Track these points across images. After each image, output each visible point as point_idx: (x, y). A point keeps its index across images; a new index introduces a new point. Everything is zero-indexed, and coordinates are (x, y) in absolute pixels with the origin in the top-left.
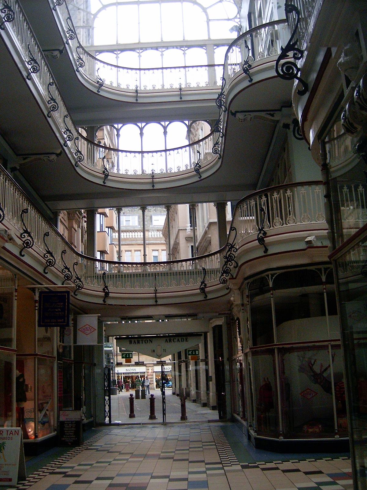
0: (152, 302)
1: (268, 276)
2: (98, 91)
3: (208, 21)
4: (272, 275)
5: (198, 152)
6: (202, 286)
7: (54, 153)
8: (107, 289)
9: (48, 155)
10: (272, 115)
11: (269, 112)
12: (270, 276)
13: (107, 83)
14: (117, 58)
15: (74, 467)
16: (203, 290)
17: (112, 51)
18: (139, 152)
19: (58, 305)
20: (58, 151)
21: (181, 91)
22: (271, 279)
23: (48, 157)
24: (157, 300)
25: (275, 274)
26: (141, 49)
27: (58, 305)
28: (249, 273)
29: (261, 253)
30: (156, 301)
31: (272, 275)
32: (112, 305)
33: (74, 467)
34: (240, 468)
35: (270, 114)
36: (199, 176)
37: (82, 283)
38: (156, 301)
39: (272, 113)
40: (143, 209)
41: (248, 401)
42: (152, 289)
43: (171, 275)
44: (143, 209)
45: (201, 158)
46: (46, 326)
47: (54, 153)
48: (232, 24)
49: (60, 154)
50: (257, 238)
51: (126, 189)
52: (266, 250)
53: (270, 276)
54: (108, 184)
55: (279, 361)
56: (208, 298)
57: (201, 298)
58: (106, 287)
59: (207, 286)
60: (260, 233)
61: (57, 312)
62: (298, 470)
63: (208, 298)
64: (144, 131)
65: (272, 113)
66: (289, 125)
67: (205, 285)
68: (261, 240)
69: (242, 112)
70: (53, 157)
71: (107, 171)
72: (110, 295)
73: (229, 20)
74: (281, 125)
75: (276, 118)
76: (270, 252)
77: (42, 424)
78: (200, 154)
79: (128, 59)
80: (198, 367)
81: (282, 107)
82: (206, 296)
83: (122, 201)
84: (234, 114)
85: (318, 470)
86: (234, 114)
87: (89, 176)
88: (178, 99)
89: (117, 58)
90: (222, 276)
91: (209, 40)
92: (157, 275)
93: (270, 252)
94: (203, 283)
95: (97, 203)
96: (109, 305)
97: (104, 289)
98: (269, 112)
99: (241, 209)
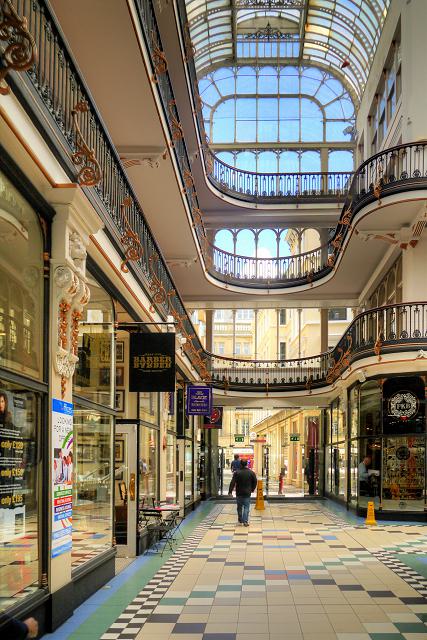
3: (325, 121)
14: (235, 158)
15: (122, 629)
17: (230, 151)
18: (254, 259)
26: (258, 149)
33: (122, 629)
34: (327, 567)
40: (256, 311)
44: (256, 311)
46: (106, 335)
48: (346, 125)
55: (42, 229)
62: (351, 549)
73: (344, 120)
77: (212, 421)
79: (246, 161)
80: (396, 600)
83: (238, 304)
85: (385, 589)
89: (235, 158)
91: (325, 142)
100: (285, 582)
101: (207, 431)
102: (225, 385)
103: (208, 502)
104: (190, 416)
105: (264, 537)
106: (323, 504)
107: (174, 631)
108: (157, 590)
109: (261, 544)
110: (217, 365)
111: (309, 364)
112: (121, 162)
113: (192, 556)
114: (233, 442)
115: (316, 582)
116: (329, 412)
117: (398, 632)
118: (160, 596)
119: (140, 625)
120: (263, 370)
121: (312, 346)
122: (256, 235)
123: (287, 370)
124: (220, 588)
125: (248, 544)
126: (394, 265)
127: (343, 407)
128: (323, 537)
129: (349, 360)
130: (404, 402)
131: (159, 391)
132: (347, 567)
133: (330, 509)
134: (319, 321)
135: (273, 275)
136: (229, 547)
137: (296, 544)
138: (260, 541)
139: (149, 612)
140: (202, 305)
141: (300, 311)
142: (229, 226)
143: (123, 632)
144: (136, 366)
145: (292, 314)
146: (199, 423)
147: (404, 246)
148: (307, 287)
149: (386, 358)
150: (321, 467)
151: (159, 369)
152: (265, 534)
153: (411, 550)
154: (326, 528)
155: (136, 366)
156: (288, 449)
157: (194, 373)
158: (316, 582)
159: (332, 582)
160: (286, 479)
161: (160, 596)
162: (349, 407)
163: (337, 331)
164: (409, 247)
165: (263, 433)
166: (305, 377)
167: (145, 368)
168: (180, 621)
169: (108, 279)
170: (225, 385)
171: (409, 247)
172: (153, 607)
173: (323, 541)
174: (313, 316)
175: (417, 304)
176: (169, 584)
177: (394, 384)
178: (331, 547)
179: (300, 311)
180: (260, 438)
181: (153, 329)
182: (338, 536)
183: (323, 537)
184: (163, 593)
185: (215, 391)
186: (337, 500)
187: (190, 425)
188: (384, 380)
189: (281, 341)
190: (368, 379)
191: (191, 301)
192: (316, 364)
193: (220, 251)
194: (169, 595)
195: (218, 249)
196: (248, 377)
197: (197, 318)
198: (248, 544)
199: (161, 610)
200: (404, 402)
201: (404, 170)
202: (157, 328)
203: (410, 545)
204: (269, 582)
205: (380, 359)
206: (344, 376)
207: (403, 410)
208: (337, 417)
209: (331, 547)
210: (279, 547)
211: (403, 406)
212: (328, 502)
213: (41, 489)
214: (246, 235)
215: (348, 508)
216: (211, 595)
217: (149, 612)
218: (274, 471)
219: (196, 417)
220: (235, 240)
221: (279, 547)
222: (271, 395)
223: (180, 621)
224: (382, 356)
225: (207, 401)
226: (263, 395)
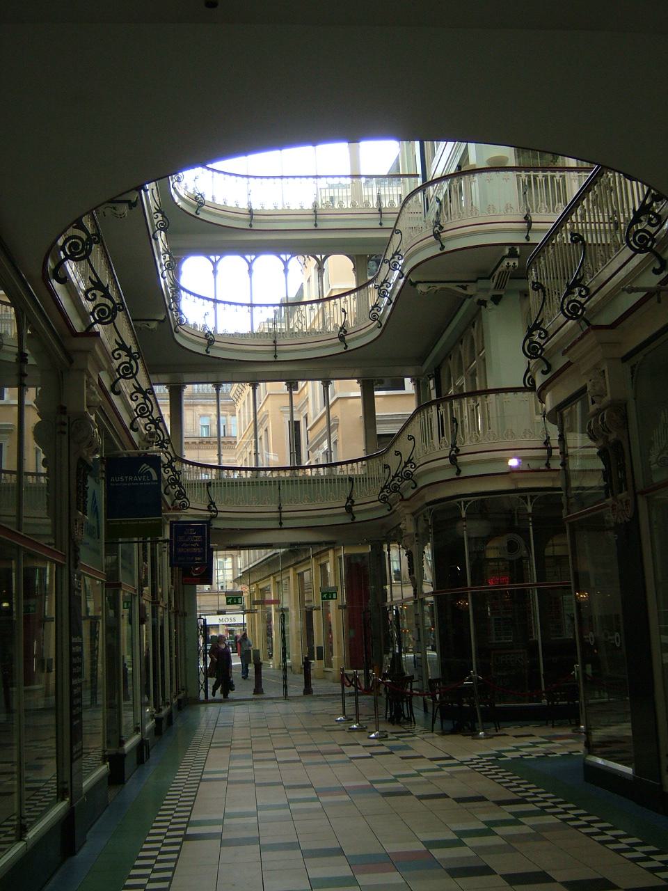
0: (275, 524)
1: (460, 503)
2: (196, 212)
4: (466, 503)
5: (344, 311)
6: (341, 333)
7: (154, 320)
8: (215, 507)
9: (148, 322)
10: (465, 288)
11: (460, 284)
12: (463, 503)
13: (208, 198)
16: (349, 509)
19: (195, 539)
20: (162, 317)
21: (316, 214)
22: (465, 507)
23: (148, 325)
24: (282, 521)
25: (470, 501)
27: (195, 539)
28: (429, 498)
29: (451, 474)
30: (281, 524)
31: (466, 503)
32: (219, 529)
33: (165, 838)
35: (462, 287)
36: (344, 346)
37: (188, 501)
38: (281, 524)
39: (465, 284)
41: (126, 647)
42: (275, 507)
43: (292, 484)
45: (346, 319)
47: (154, 320)
49: (163, 321)
50: (448, 455)
51: (237, 360)
52: (459, 471)
53: (463, 503)
54: (213, 353)
56: (356, 520)
57: (347, 519)
58: (213, 503)
59: (355, 504)
60: (452, 450)
61: (193, 547)
62: (432, 759)
63: (356, 520)
64: (254, 267)
65: (465, 284)
66: (486, 301)
67: (353, 501)
68: (453, 459)
69: (425, 282)
70: (154, 325)
71: (211, 334)
72: (220, 515)
74: (476, 300)
75: (469, 292)
76: (462, 475)
78: (345, 314)
81: (479, 278)
82: (354, 517)
84: (414, 284)
86: (414, 284)
87: (196, 346)
88: (312, 226)
90: (381, 493)
92: (281, 483)
93: (462, 475)
94: (350, 498)
95: (186, 377)
96: (215, 528)
97: (209, 507)
98: (460, 284)
99: (424, 415)
100: (346, 798)
115: (386, 794)
117: (457, 838)
122: (250, 264)
132: (426, 777)
138: (298, 758)
140: (165, 378)
142: (206, 251)
147: (482, 303)
153: (516, 755)
158: (386, 794)
159: (408, 793)
164: (490, 305)
169: (23, 427)
171: (490, 305)
178: (402, 758)
183: (389, 747)
191: (190, 372)
193: (191, 293)
201: (336, 322)
203: (517, 749)
204: (322, 799)
208: (396, 559)
209: (402, 758)
213: (245, 349)
214: (232, 264)
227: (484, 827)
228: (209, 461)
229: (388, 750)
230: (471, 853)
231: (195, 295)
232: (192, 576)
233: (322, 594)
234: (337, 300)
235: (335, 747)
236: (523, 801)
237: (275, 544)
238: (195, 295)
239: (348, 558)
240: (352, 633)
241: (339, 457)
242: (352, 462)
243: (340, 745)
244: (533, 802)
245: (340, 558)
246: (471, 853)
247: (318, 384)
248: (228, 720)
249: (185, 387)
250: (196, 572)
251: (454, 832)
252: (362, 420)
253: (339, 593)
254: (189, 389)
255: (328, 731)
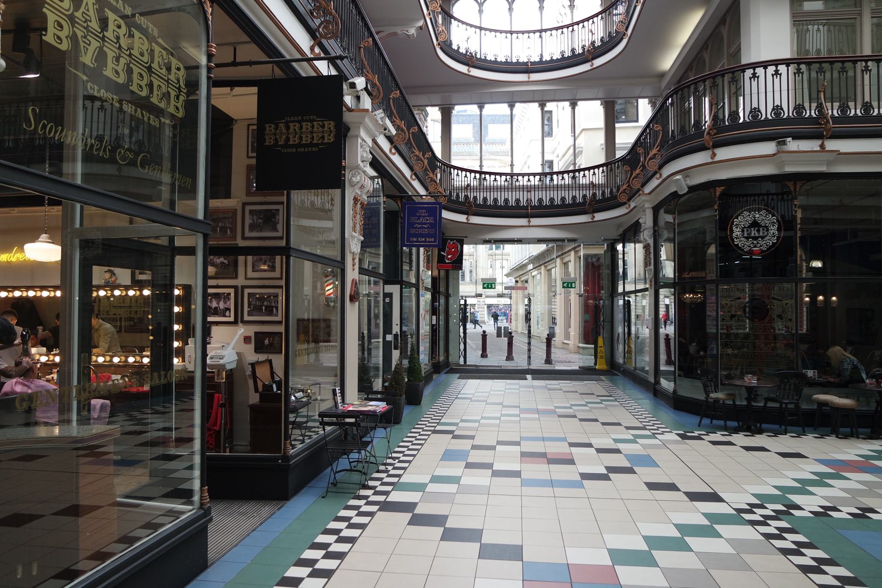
33: (360, 507)
95: (455, 97)
101: (442, 273)
102: (468, 207)
103: (443, 377)
104: (414, 250)
105: (524, 455)
106: (611, 381)
107: (411, 523)
108: (411, 447)
109: (517, 474)
110: (459, 180)
111: (584, 179)
112: (377, 37)
113: (435, 432)
114: (480, 290)
116: (620, 247)
118: (395, 480)
119: (371, 514)
120: (523, 188)
121: (593, 152)
123: (558, 187)
124: (482, 418)
125: (496, 474)
126: (723, 21)
127: (646, 235)
128: (628, 457)
129: (658, 161)
130: (755, 224)
131: (257, 158)
133: (624, 390)
134: (601, 123)
135: (528, 162)
136: (455, 480)
137: (586, 476)
138: (516, 467)
139: (381, 498)
140: (437, 99)
141: (574, 105)
143: (317, 566)
144: (269, 141)
145: (560, 110)
146: (428, 260)
148: (586, 67)
149: (724, 153)
150: (607, 326)
151: (311, 145)
152: (528, 447)
154: (628, 435)
155: (269, 141)
156: (559, 300)
157: (416, 184)
160: (557, 340)
161: (395, 480)
162: (656, 235)
163: (627, 136)
165: (524, 278)
166: (584, 196)
167: (286, 145)
168: (418, 511)
170: (468, 207)
172: (387, 493)
173: (630, 471)
174: (592, 112)
175: (776, 63)
176: (410, 458)
177: (735, 193)
178: (653, 486)
179: (574, 105)
180: (519, 285)
181: (304, 70)
182: (655, 455)
183: (628, 457)
184: (399, 476)
185: (446, 214)
186: (636, 379)
187: (414, 268)
188: (719, 190)
189: (547, 158)
190: (692, 189)
192: (598, 178)
194: (406, 478)
195: (456, 19)
196: (501, 197)
197: (431, 123)
198: (496, 474)
199: (396, 496)
200: (755, 224)
202: (315, 69)
205: (714, 155)
206: (648, 189)
207: (755, 238)
208: (632, 255)
210: (552, 483)
211: (754, 233)
212: (620, 379)
215: (656, 392)
216: (478, 421)
217: (381, 498)
218: (540, 330)
219: (422, 249)
220: (481, 11)
221: (552, 483)
222: (535, 221)
223: (418, 511)
224: (717, 151)
225: (433, 226)
226: (523, 221)
227: (705, 522)
228: (586, 385)
229: (626, 464)
230: (696, 564)
231: (467, 24)
232: (445, 262)
233: (563, 283)
234: (587, 172)
235: (562, 449)
236: (644, 428)
237: (524, 239)
238: (467, 24)
239: (586, 257)
240: (587, 317)
241: (582, 163)
242: (594, 168)
243: (572, 445)
244: (650, 430)
245: (580, 258)
246: (696, 564)
247: (567, 104)
248: (474, 403)
249: (453, 108)
250: (448, 259)
251: (676, 526)
252: (604, 147)
253: (577, 283)
254: (458, 109)
255: (560, 416)
